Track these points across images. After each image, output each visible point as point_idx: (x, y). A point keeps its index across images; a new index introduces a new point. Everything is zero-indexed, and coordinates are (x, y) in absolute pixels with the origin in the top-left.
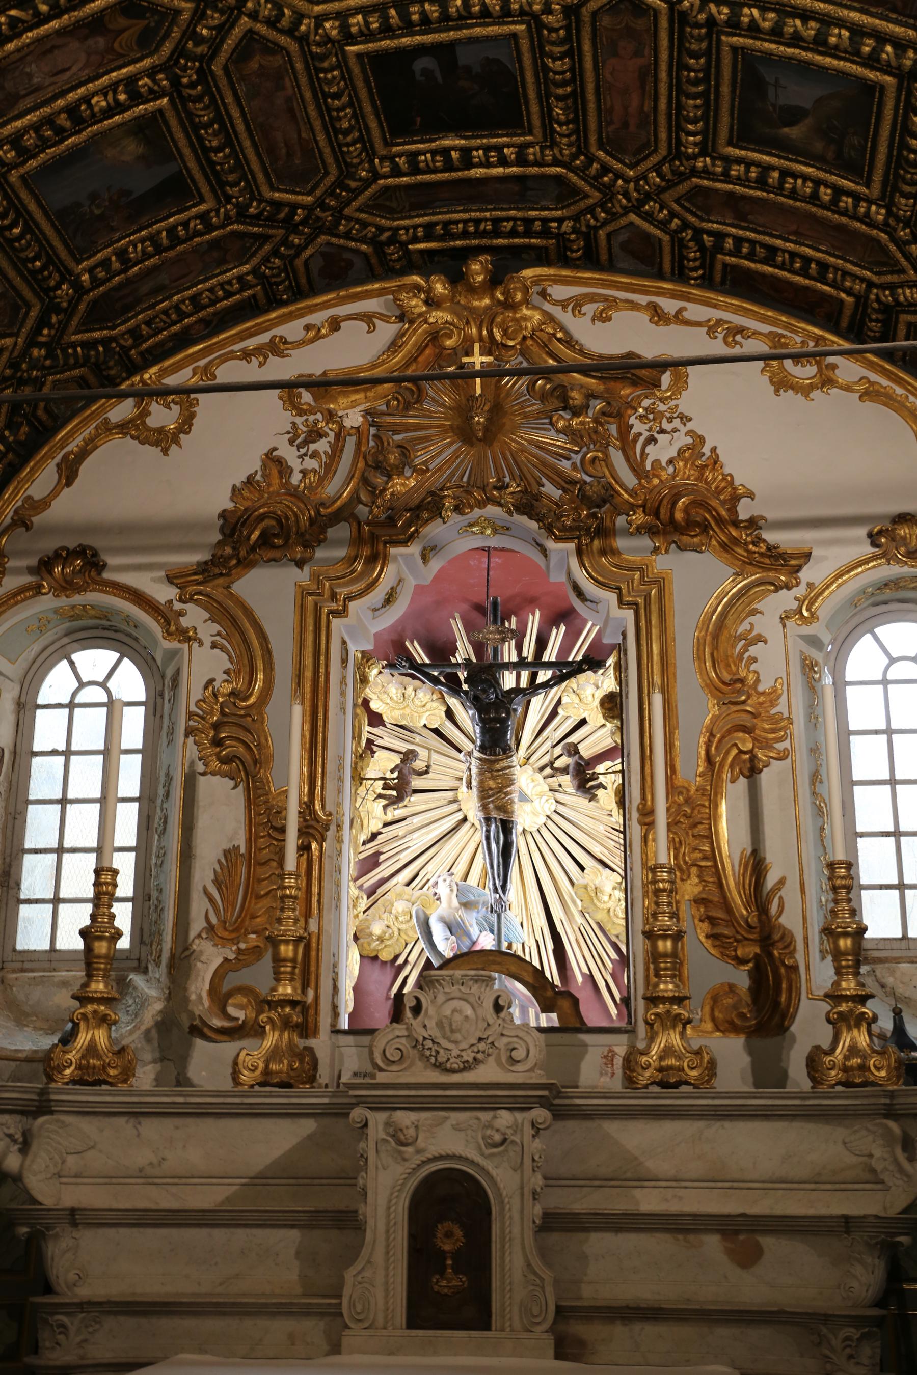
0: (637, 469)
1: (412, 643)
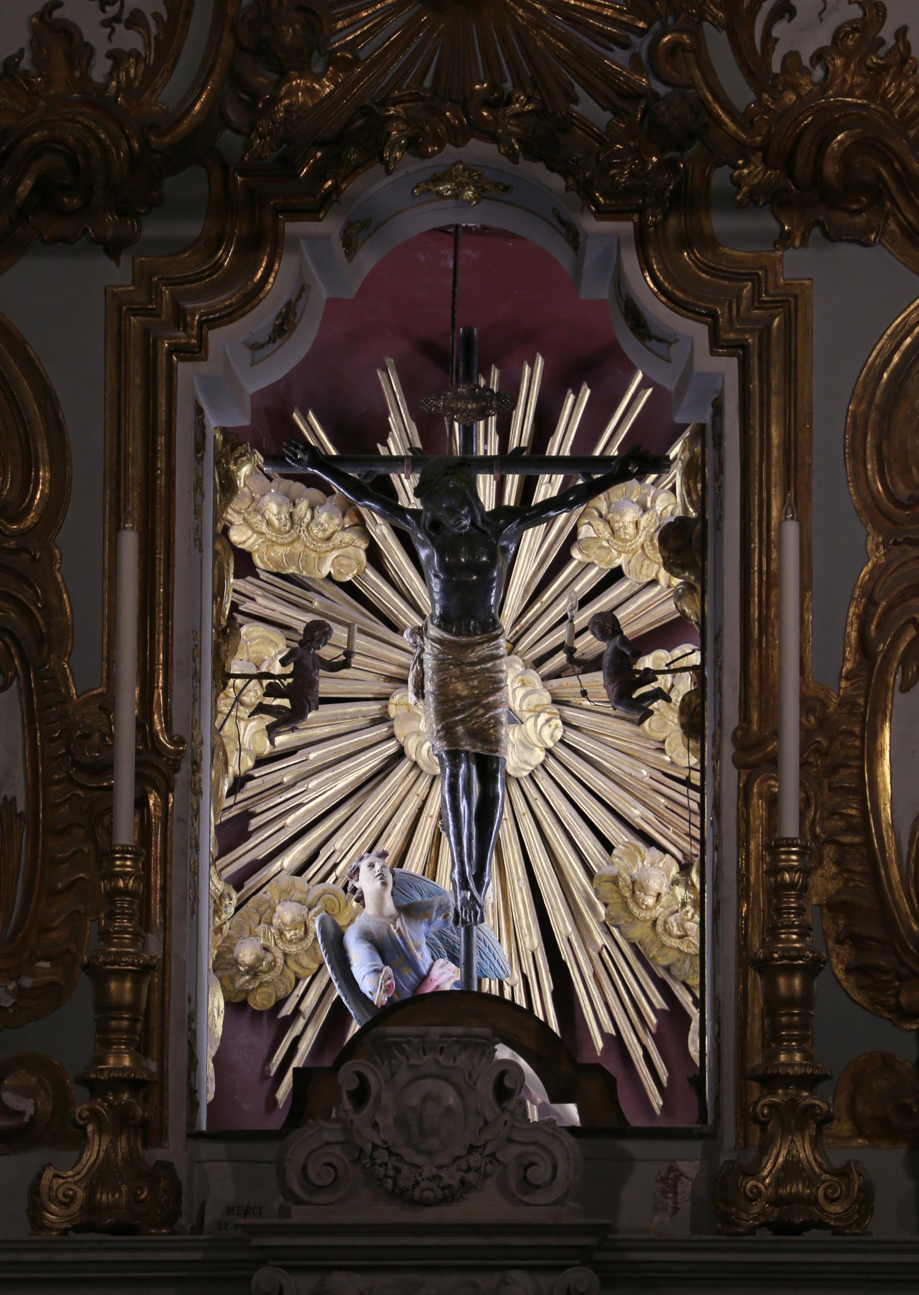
0: (754, 68)
1: (305, 416)
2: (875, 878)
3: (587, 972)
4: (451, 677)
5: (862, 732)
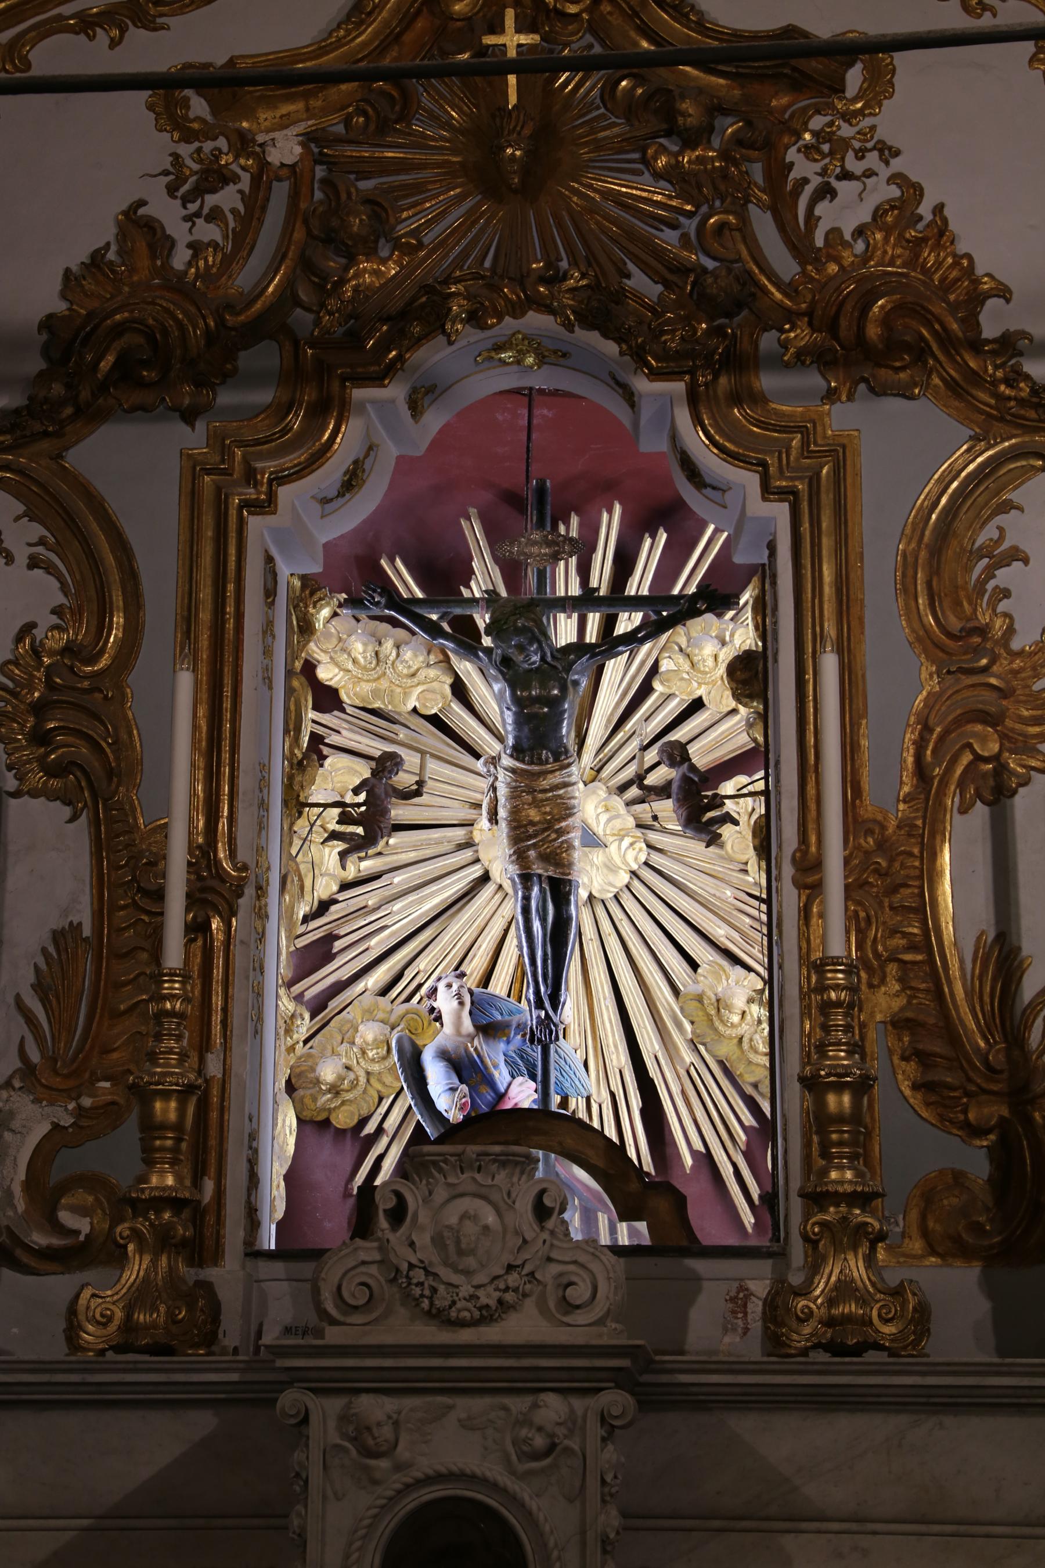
0: (799, 245)
1: (392, 561)
2: (938, 995)
3: (675, 1089)
4: (523, 804)
5: (922, 853)
